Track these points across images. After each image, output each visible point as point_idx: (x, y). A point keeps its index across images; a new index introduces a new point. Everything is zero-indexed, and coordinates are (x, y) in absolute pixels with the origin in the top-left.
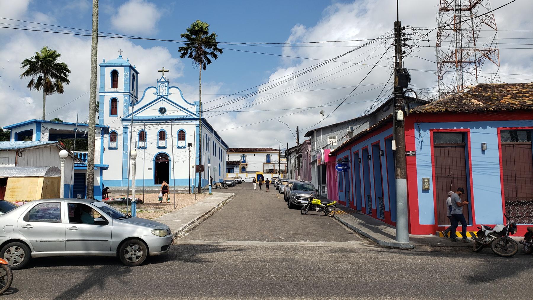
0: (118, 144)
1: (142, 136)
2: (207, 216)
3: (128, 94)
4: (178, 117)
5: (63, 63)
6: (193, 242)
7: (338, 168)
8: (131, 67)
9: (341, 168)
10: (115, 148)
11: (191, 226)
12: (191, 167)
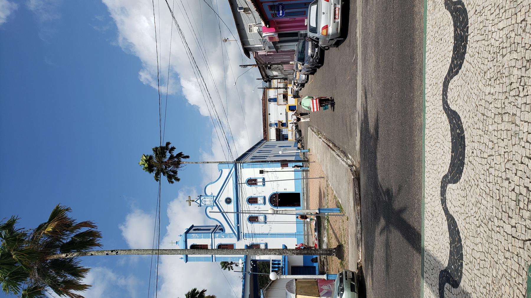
0: (262, 242)
2: (331, 145)
3: (213, 234)
5: (186, 295)
6: (358, 147)
7: (281, 15)
8: (187, 233)
9: (281, 12)
11: (342, 155)
12: (283, 170)
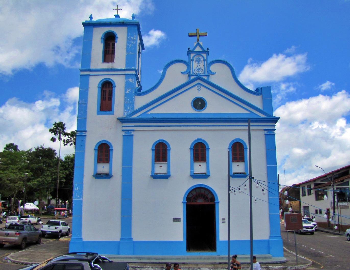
1: (161, 152)
4: (210, 117)
10: (108, 176)
